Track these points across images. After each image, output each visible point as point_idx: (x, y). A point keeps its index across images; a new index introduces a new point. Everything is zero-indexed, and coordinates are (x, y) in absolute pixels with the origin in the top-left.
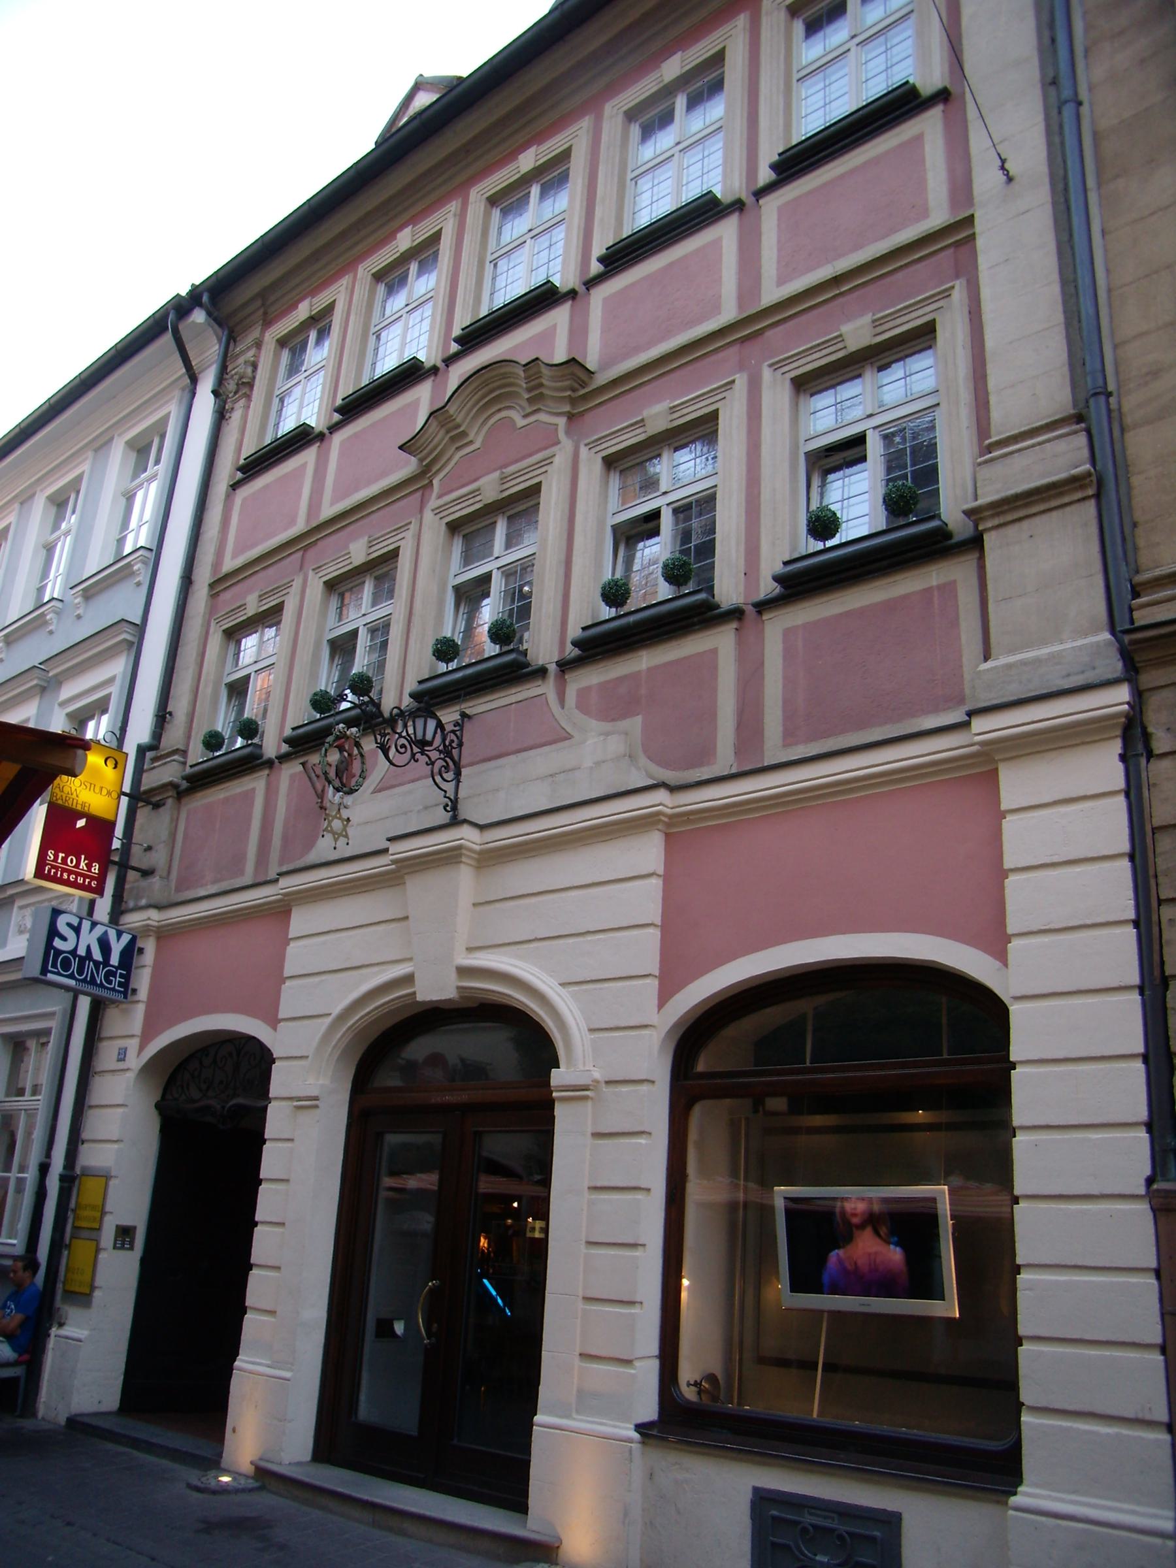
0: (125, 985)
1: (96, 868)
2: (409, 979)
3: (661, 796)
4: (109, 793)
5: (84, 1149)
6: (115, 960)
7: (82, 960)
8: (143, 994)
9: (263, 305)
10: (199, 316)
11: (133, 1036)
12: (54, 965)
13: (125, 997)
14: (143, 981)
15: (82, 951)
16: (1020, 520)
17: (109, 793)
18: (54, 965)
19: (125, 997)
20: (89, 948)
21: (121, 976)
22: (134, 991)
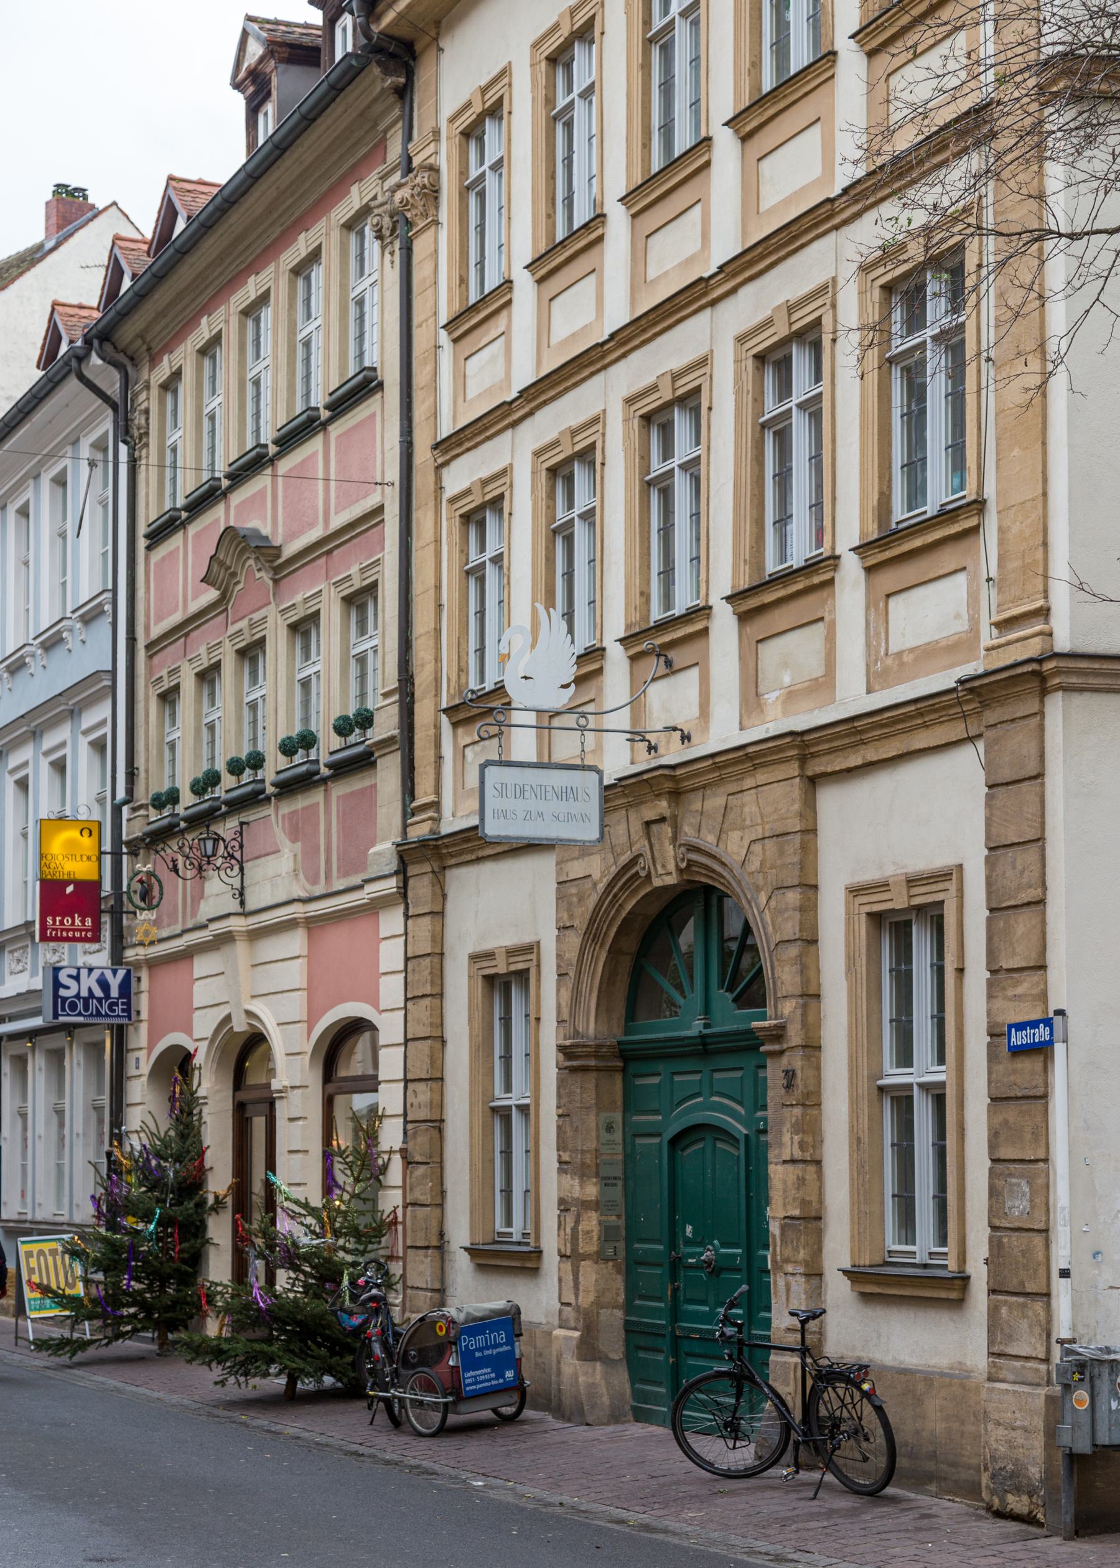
0: (128, 1010)
1: (89, 922)
4: (89, 858)
6: (114, 992)
7: (86, 1001)
8: (144, 1015)
9: (144, 342)
10: (95, 360)
11: (141, 1049)
12: (63, 1009)
13: (130, 1019)
14: (143, 1004)
15: (84, 993)
17: (89, 858)
18: (63, 1009)
19: (130, 1019)
20: (90, 990)
21: (123, 1004)
22: (138, 1013)
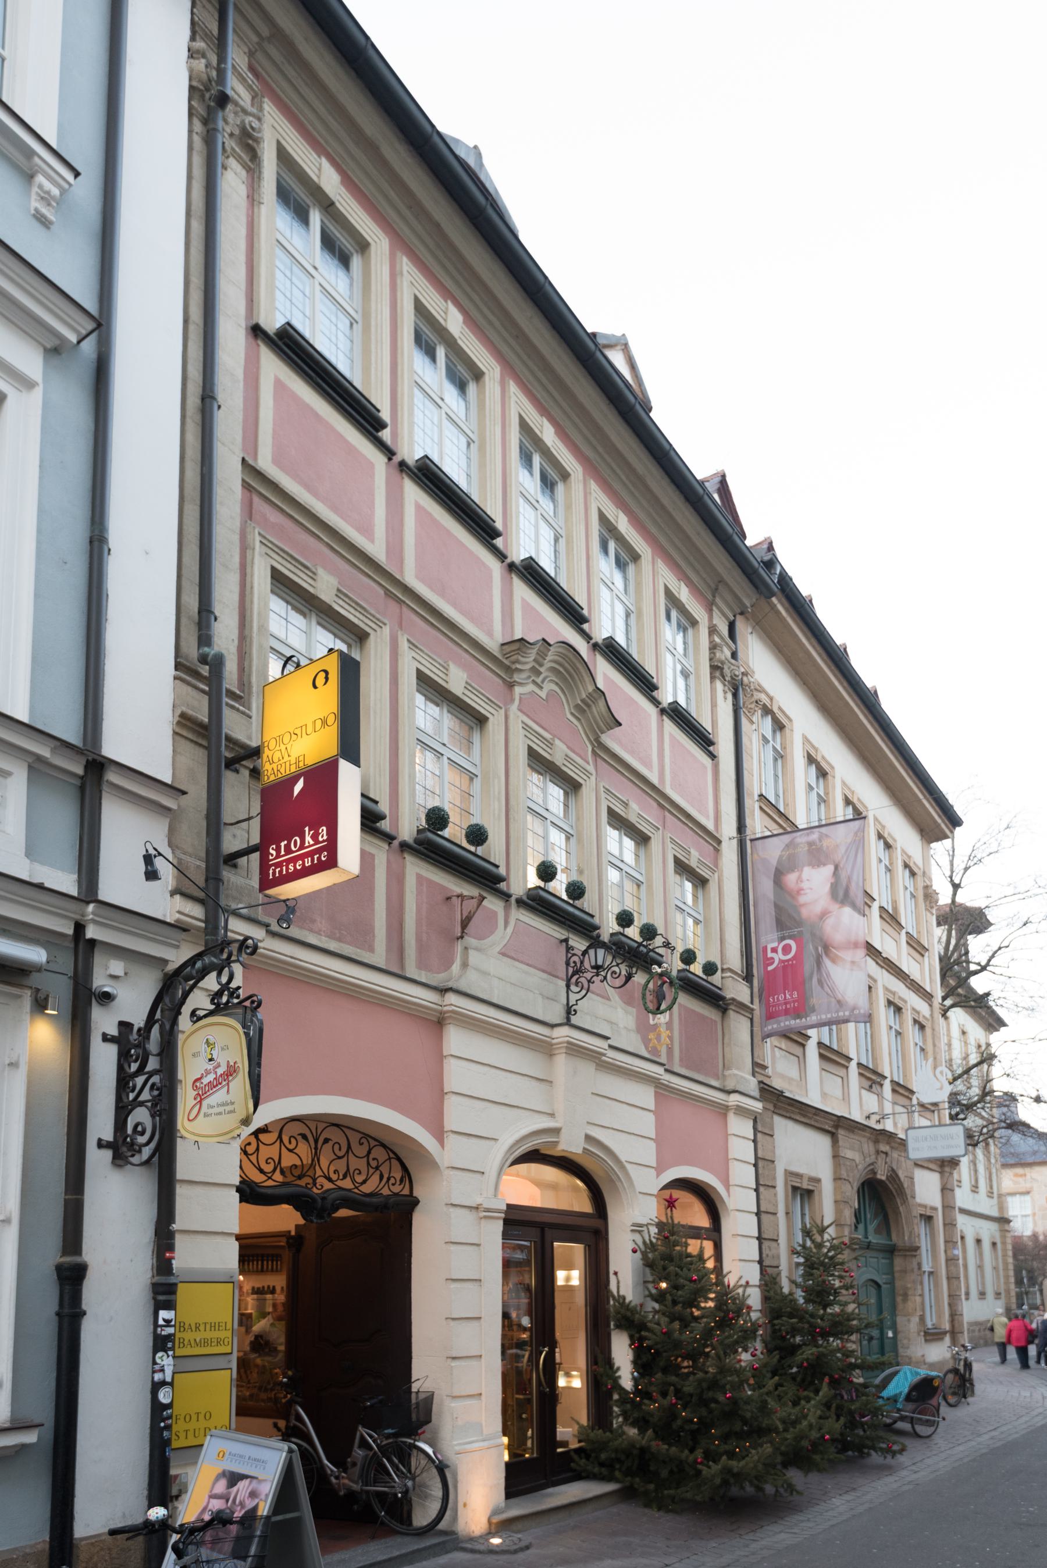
2: (556, 1131)
3: (660, 1070)
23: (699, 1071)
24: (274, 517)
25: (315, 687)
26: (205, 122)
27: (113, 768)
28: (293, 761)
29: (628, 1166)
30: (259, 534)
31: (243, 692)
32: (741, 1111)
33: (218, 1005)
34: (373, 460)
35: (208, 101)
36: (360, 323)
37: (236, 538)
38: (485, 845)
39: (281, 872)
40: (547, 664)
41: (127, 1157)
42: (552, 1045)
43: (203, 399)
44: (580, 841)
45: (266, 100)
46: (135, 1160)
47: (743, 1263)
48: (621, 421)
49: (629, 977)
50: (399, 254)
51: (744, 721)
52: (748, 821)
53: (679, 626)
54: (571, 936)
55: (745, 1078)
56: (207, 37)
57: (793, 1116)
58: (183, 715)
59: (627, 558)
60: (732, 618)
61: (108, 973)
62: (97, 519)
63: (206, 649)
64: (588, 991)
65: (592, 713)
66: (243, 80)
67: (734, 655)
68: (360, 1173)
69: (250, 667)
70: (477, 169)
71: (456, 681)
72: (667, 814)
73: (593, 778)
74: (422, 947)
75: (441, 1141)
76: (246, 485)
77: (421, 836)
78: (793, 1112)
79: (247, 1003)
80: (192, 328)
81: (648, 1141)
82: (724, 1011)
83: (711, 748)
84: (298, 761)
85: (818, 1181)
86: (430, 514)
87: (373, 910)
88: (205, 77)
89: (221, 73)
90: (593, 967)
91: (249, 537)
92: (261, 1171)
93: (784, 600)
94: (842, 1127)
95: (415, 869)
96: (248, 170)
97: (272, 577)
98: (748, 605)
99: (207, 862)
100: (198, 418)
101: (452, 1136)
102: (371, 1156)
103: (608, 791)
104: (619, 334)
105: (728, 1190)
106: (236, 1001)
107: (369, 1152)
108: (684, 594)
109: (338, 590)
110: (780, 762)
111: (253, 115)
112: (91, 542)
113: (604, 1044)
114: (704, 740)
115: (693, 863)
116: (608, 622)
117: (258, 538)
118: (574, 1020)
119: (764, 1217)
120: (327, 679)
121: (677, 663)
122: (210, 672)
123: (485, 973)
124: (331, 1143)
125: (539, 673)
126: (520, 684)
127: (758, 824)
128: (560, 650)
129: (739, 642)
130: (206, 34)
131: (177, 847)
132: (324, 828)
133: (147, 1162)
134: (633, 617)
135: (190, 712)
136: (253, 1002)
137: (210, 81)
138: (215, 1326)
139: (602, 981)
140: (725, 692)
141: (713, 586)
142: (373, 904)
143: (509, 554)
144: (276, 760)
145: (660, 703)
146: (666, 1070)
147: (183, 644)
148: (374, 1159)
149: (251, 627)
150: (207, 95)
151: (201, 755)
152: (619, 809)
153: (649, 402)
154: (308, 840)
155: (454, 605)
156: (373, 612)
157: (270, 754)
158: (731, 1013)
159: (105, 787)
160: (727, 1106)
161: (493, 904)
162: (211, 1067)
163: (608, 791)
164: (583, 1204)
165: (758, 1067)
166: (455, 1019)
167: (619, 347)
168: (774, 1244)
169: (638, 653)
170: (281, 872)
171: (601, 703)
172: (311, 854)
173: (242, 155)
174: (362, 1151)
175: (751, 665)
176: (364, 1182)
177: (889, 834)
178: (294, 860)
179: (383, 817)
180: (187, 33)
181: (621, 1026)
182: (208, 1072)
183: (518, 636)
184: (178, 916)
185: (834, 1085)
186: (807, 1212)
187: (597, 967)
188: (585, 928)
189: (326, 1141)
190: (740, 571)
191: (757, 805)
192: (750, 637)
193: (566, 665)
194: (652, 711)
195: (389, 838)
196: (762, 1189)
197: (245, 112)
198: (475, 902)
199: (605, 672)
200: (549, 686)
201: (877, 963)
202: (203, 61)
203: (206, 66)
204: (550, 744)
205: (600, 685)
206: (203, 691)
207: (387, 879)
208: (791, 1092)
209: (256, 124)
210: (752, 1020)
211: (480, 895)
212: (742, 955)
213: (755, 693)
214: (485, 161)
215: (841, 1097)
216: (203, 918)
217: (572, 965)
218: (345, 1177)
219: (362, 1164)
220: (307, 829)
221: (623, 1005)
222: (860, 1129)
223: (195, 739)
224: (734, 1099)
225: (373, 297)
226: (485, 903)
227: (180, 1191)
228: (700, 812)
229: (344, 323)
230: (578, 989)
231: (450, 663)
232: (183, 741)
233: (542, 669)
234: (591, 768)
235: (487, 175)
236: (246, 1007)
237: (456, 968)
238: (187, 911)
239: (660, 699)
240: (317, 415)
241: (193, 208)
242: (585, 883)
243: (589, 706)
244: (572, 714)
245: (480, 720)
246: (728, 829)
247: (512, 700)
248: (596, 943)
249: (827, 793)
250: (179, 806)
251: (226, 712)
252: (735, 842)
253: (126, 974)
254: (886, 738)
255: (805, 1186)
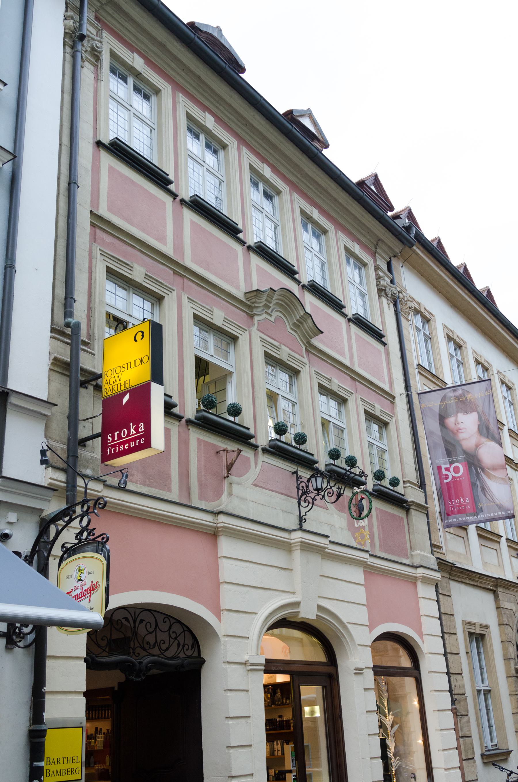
2: (297, 604)
3: (366, 556)
5: (49, 700)
16: (417, 510)
23: (393, 554)
24: (108, 239)
25: (136, 340)
26: (72, 47)
27: (14, 394)
28: (122, 384)
29: (349, 626)
30: (100, 250)
31: (89, 339)
32: (426, 580)
33: (80, 540)
34: (165, 201)
35: (74, 38)
36: (156, 129)
37: (87, 254)
38: (240, 415)
39: (115, 450)
40: (274, 302)
41: (16, 642)
42: (291, 544)
43: (69, 184)
44: (301, 407)
45: (104, 31)
46: (21, 644)
47: (437, 693)
48: (311, 161)
49: (339, 495)
50: (177, 93)
51: (403, 320)
52: (412, 383)
53: (355, 266)
54: (299, 469)
55: (426, 557)
56: (74, 8)
57: (464, 581)
58: (55, 359)
59: (320, 232)
60: (389, 260)
61: (7, 521)
62: (9, 256)
63: (69, 320)
64: (313, 504)
65: (304, 327)
66: (92, 24)
67: (392, 281)
68: (164, 643)
69: (94, 324)
70: (219, 38)
71: (218, 317)
72: (357, 383)
73: (307, 366)
74: (201, 485)
75: (219, 617)
76: (93, 225)
77: (200, 414)
78: (464, 578)
79: (100, 539)
80: (64, 148)
81: (361, 607)
82: (407, 510)
83: (383, 339)
84: (125, 383)
85: (487, 627)
86: (199, 225)
87: (170, 464)
88: (73, 28)
89: (81, 25)
90: (315, 490)
91: (94, 252)
92: (99, 646)
93: (420, 247)
94: (500, 586)
95: (196, 436)
96: (95, 66)
97: (107, 271)
98: (398, 252)
99: (68, 445)
100: (66, 194)
101: (226, 613)
102: (172, 630)
103: (317, 373)
104: (306, 109)
105: (422, 639)
106: (91, 537)
107: (170, 628)
108: (357, 249)
109: (146, 275)
110: (429, 342)
111: (98, 41)
112: (5, 268)
113: (325, 541)
114: (378, 335)
115: (378, 413)
116: (310, 271)
117: (99, 252)
118: (305, 526)
119: (449, 656)
120: (143, 336)
121: (356, 291)
122: (72, 332)
123: (243, 499)
124: (144, 623)
125: (269, 307)
126: (257, 315)
127: (419, 384)
128: (281, 293)
129: (394, 275)
130: (73, 7)
131: (50, 438)
132: (142, 424)
133: (26, 647)
134: (326, 266)
135: (59, 357)
136: (103, 538)
137: (75, 29)
138: (70, 760)
139: (321, 499)
140: (389, 304)
141: (375, 243)
142: (170, 461)
143: (247, 242)
144: (111, 382)
145: (347, 316)
146: (370, 555)
147: (55, 317)
148: (173, 632)
149: (95, 302)
150: (74, 35)
151: (65, 381)
152: (325, 384)
153: (328, 142)
154: (132, 431)
155: (216, 274)
156: (166, 284)
157: (108, 379)
158: (412, 511)
159: (9, 406)
160: (416, 577)
161: (247, 453)
162: (79, 585)
163: (317, 373)
164: (321, 657)
165: (435, 547)
166: (224, 531)
167: (306, 116)
168: (459, 677)
169: (331, 286)
170: (115, 450)
171: (310, 321)
172: (134, 440)
173: (91, 59)
174: (165, 627)
175: (404, 286)
176: (167, 649)
177: (509, 381)
178: (123, 443)
179: (175, 406)
180: (63, 8)
181: (337, 526)
182: (76, 588)
183: (255, 288)
184: (50, 481)
185: (491, 555)
186: (482, 651)
187: (317, 490)
188: (308, 463)
189: (142, 621)
190: (391, 234)
191: (416, 372)
192: (401, 269)
193: (286, 300)
194: (343, 321)
195: (179, 418)
196: (446, 636)
197: (93, 39)
198: (235, 454)
199: (310, 302)
200: (275, 314)
201: (511, 467)
202: (72, 21)
203: (74, 23)
204: (278, 348)
205: (308, 311)
206: (67, 343)
207: (178, 443)
208: (460, 563)
209: (99, 45)
210: (427, 515)
211: (238, 449)
212: (416, 471)
213: (408, 303)
214: (224, 33)
215: (497, 564)
216: (66, 481)
217: (301, 488)
218: (154, 646)
219: (165, 636)
220: (131, 424)
221: (337, 512)
222: (513, 587)
223: (61, 372)
224: (420, 572)
225: (163, 116)
226: (242, 453)
227: (50, 664)
228: (379, 379)
229: (147, 130)
230: (307, 504)
231: (214, 308)
232: (54, 373)
233: (271, 305)
234: (305, 360)
235: (225, 39)
236: (99, 542)
237: (224, 497)
238: (55, 478)
239: (347, 313)
240: (133, 182)
241: (65, 89)
242: (306, 434)
243: (301, 323)
244: (291, 328)
245: (234, 339)
246: (399, 389)
247: (253, 325)
248: (316, 473)
249: (463, 359)
250: (52, 413)
251: (82, 354)
252: (404, 397)
253: (17, 520)
254: (497, 321)
255: (478, 631)
